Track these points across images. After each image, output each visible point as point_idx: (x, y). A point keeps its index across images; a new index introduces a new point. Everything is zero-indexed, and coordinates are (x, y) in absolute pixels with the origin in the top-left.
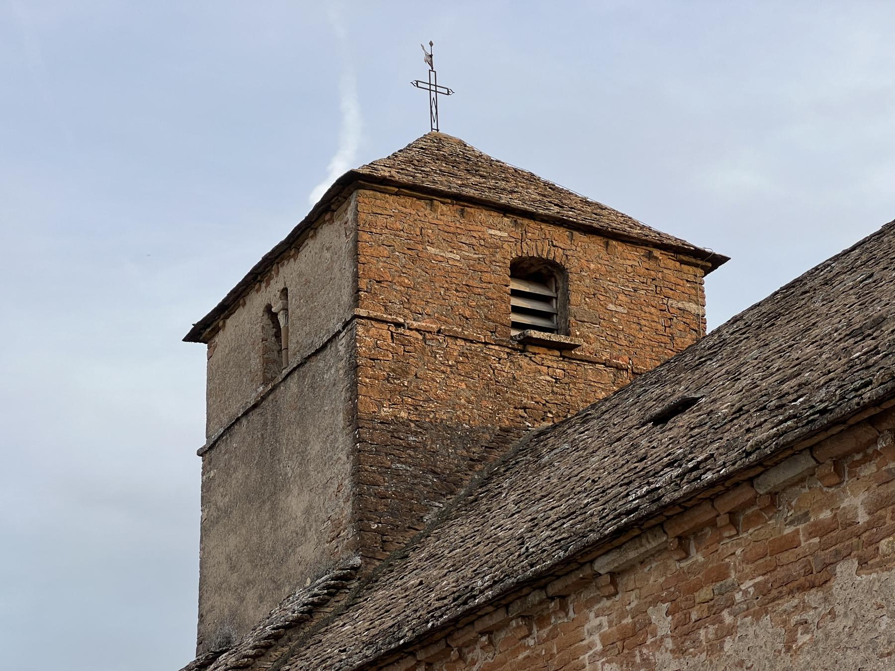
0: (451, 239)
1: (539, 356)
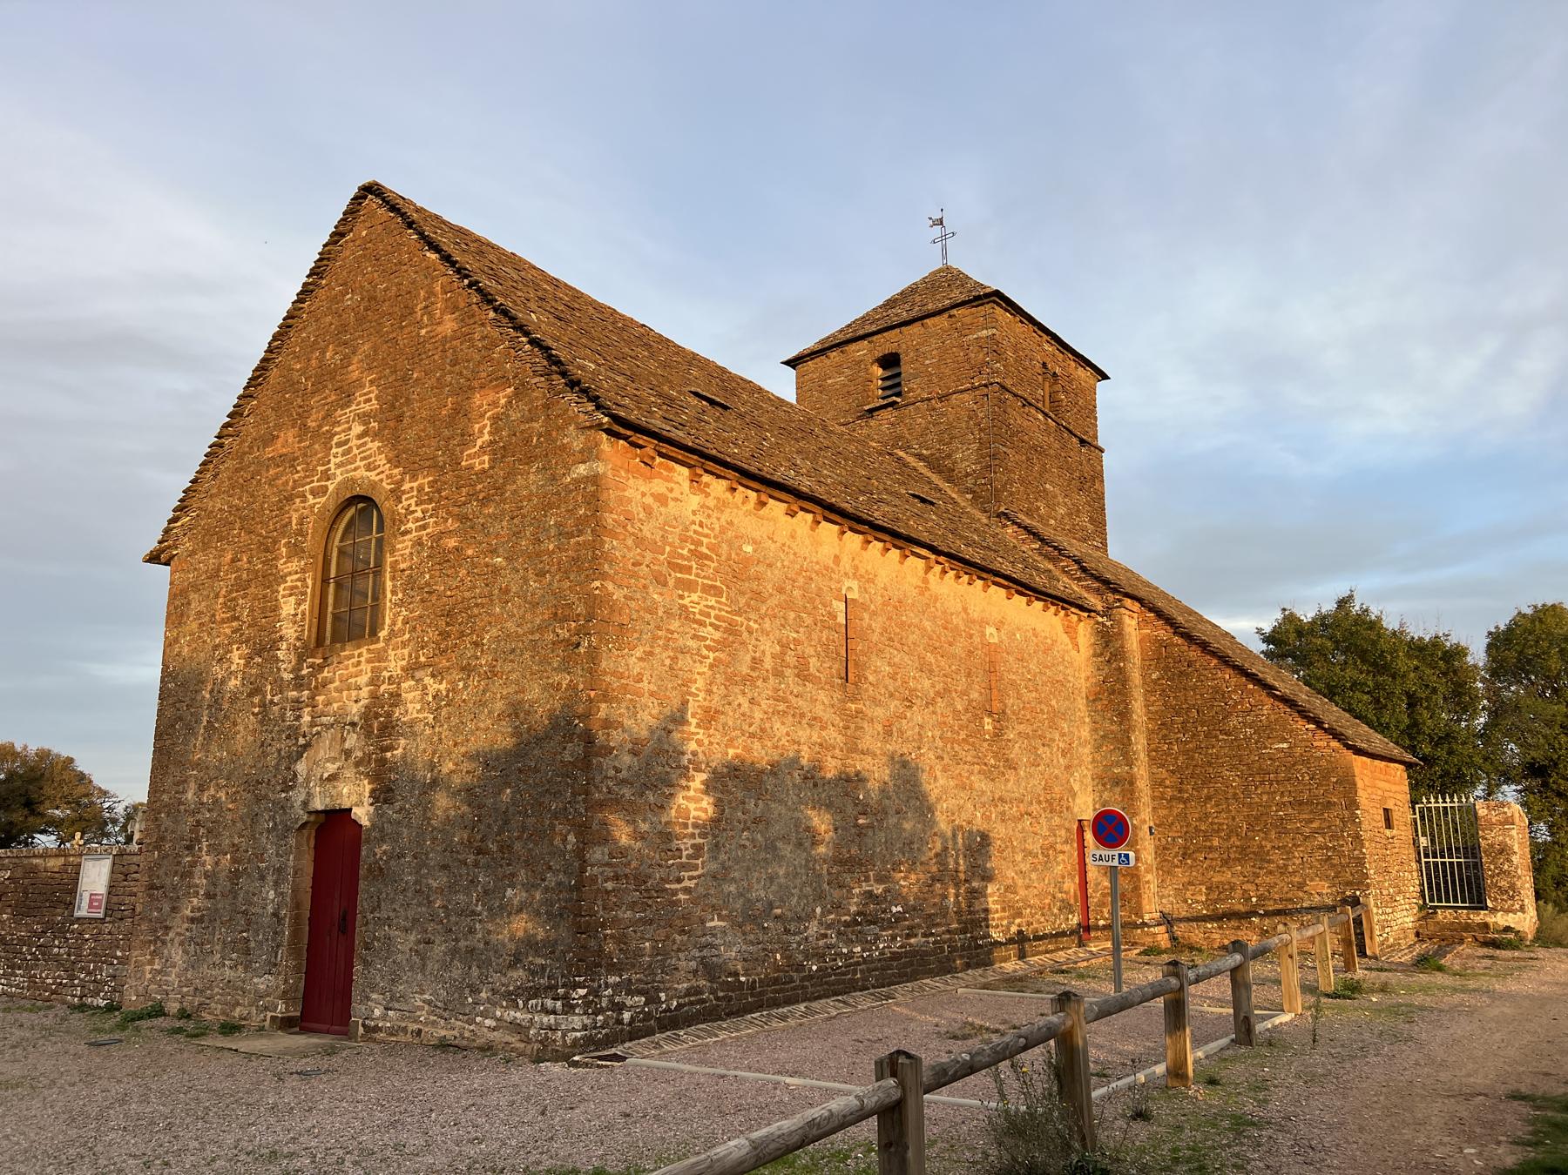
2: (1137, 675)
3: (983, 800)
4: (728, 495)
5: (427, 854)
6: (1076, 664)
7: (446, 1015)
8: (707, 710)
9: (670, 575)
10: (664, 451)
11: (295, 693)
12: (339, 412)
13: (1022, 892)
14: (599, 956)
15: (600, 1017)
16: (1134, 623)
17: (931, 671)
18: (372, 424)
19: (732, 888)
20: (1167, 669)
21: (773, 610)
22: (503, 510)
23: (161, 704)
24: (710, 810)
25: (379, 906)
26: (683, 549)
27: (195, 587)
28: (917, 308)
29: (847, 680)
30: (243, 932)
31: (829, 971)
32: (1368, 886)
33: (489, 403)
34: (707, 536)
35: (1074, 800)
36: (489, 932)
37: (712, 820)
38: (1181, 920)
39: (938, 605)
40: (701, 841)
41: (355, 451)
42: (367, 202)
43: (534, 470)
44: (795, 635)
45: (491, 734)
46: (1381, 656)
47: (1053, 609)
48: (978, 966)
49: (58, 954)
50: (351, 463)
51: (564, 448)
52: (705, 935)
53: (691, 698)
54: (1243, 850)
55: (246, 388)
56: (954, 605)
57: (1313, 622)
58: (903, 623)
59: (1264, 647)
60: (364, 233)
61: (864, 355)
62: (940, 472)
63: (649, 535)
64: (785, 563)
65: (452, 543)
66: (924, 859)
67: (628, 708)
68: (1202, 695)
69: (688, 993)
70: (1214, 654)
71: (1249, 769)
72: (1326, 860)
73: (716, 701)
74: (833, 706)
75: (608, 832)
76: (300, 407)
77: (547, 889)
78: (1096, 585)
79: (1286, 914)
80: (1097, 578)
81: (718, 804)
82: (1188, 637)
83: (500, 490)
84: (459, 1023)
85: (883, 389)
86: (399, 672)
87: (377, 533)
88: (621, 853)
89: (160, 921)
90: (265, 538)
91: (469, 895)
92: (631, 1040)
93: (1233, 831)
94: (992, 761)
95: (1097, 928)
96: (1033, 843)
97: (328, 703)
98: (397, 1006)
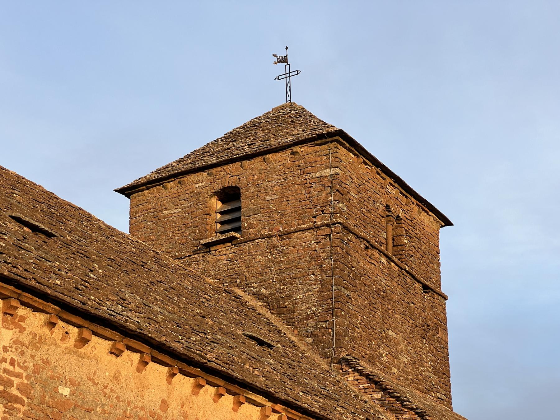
0: (175, 200)
1: (218, 251)
4: (46, 330)
28: (259, 143)
34: (18, 376)
61: (203, 187)
62: (279, 313)
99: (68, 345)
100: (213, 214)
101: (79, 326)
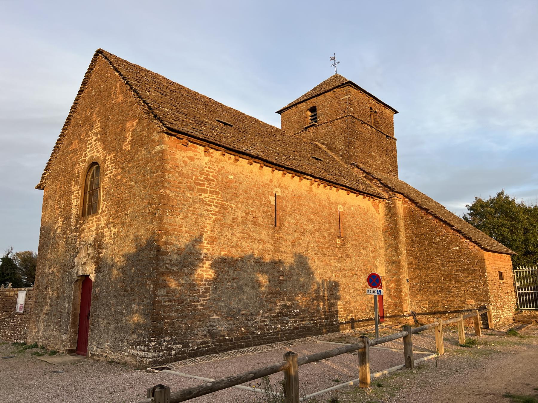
2: (402, 222)
3: (336, 270)
4: (222, 157)
5: (110, 291)
6: (378, 219)
7: (114, 350)
8: (212, 238)
9: (195, 187)
10: (191, 140)
11: (75, 233)
12: (90, 133)
13: (353, 304)
14: (161, 330)
15: (161, 353)
16: (401, 203)
17: (313, 222)
18: (98, 136)
19: (223, 304)
20: (413, 219)
21: (242, 200)
22: (135, 164)
23: (40, 238)
24: (213, 275)
25: (96, 310)
26: (201, 177)
27: (50, 197)
28: (323, 90)
29: (276, 226)
30: (59, 319)
31: (266, 334)
32: (490, 302)
33: (131, 125)
34: (212, 172)
35: (376, 269)
36: (127, 320)
37: (213, 278)
38: (419, 314)
39: (316, 197)
40: (209, 286)
41: (94, 146)
42: (99, 56)
43: (143, 149)
44: (252, 209)
45: (129, 248)
46: (513, 214)
47: (367, 198)
48: (333, 332)
49: (12, 325)
50: (93, 151)
51: (153, 140)
52: (210, 321)
53: (204, 233)
54: (442, 288)
55: (64, 126)
56: (324, 197)
57: (488, 202)
58: (301, 204)
59: (469, 212)
60: (98, 68)
61: (304, 108)
62: (331, 149)
63: (185, 172)
64: (248, 182)
65: (119, 177)
66: (309, 292)
67: (176, 237)
68: (426, 229)
69: (202, 343)
70: (430, 214)
71: (444, 257)
72: (474, 292)
73: (216, 234)
74: (269, 235)
75: (166, 284)
76: (79, 132)
77: (144, 305)
78: (386, 189)
79: (458, 312)
80: (386, 186)
81: (216, 272)
82: (421, 207)
83: (133, 157)
84: (117, 354)
85: (311, 120)
86: (104, 225)
87: (96, 177)
88: (172, 291)
89: (38, 314)
90: (68, 179)
91: (121, 306)
92: (175, 361)
93: (438, 281)
94: (340, 255)
95: (387, 317)
96: (358, 286)
97: (84, 237)
98: (100, 346)
99: (231, 162)
100: (308, 117)
101: (234, 155)
